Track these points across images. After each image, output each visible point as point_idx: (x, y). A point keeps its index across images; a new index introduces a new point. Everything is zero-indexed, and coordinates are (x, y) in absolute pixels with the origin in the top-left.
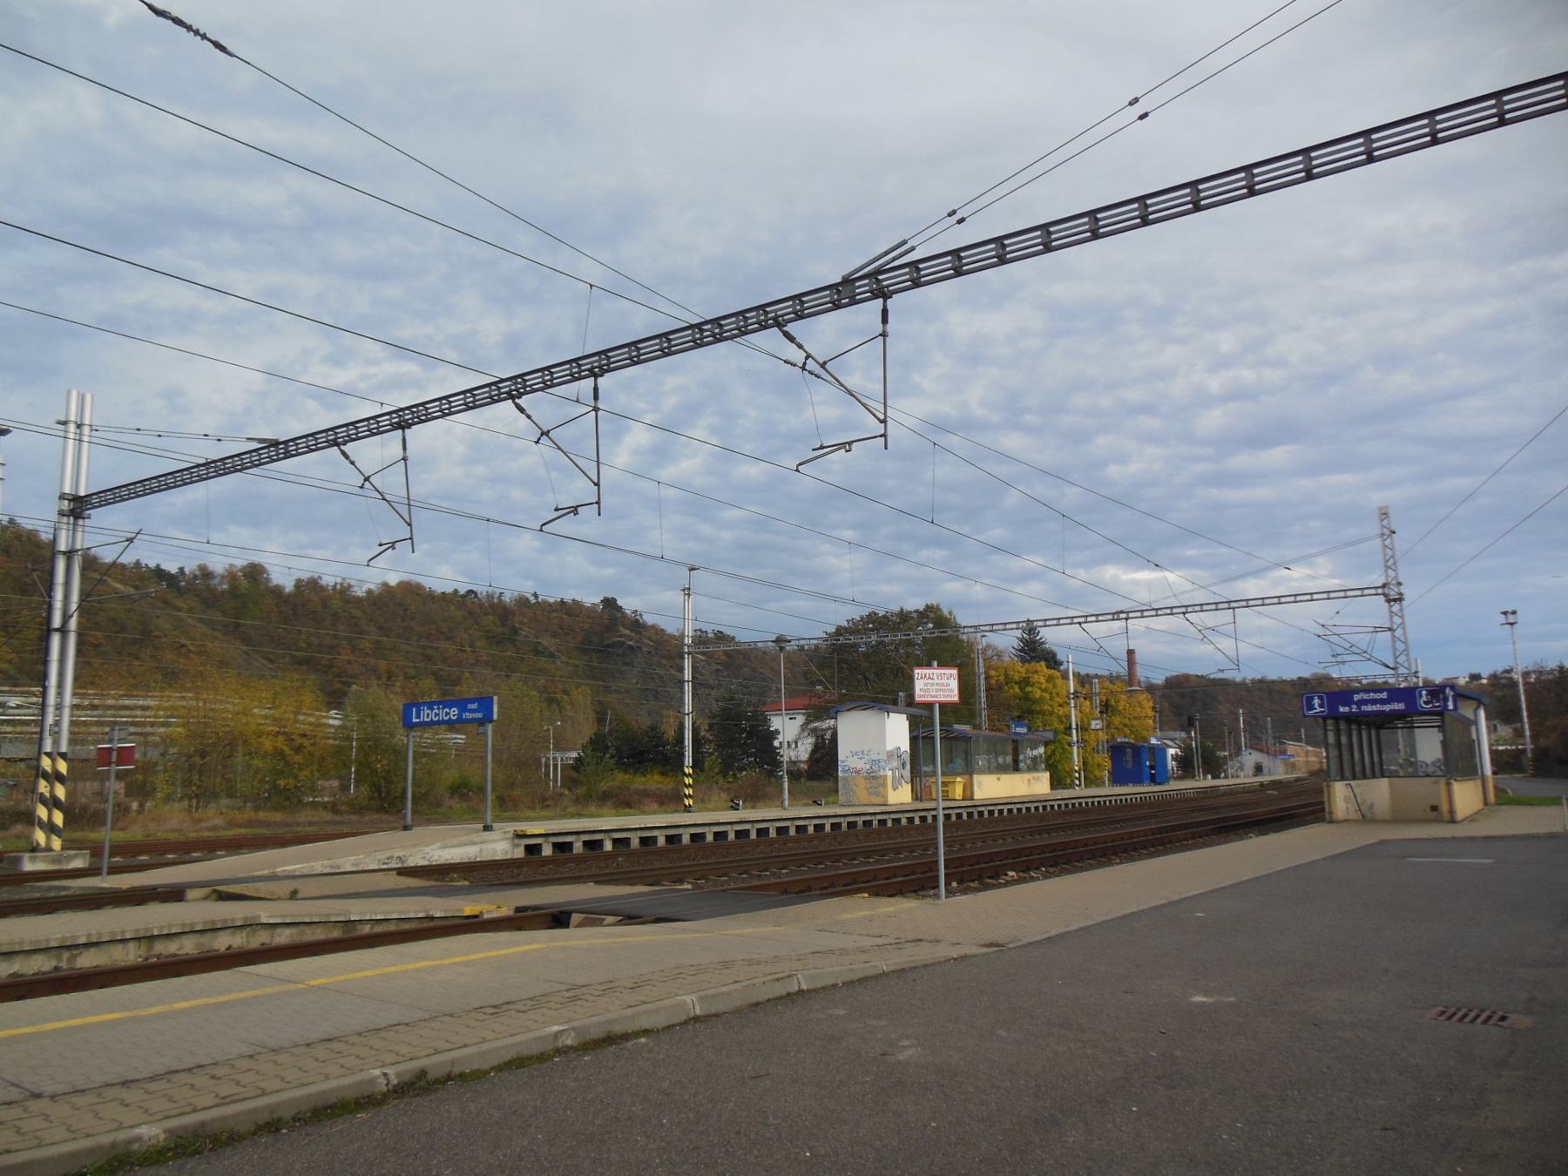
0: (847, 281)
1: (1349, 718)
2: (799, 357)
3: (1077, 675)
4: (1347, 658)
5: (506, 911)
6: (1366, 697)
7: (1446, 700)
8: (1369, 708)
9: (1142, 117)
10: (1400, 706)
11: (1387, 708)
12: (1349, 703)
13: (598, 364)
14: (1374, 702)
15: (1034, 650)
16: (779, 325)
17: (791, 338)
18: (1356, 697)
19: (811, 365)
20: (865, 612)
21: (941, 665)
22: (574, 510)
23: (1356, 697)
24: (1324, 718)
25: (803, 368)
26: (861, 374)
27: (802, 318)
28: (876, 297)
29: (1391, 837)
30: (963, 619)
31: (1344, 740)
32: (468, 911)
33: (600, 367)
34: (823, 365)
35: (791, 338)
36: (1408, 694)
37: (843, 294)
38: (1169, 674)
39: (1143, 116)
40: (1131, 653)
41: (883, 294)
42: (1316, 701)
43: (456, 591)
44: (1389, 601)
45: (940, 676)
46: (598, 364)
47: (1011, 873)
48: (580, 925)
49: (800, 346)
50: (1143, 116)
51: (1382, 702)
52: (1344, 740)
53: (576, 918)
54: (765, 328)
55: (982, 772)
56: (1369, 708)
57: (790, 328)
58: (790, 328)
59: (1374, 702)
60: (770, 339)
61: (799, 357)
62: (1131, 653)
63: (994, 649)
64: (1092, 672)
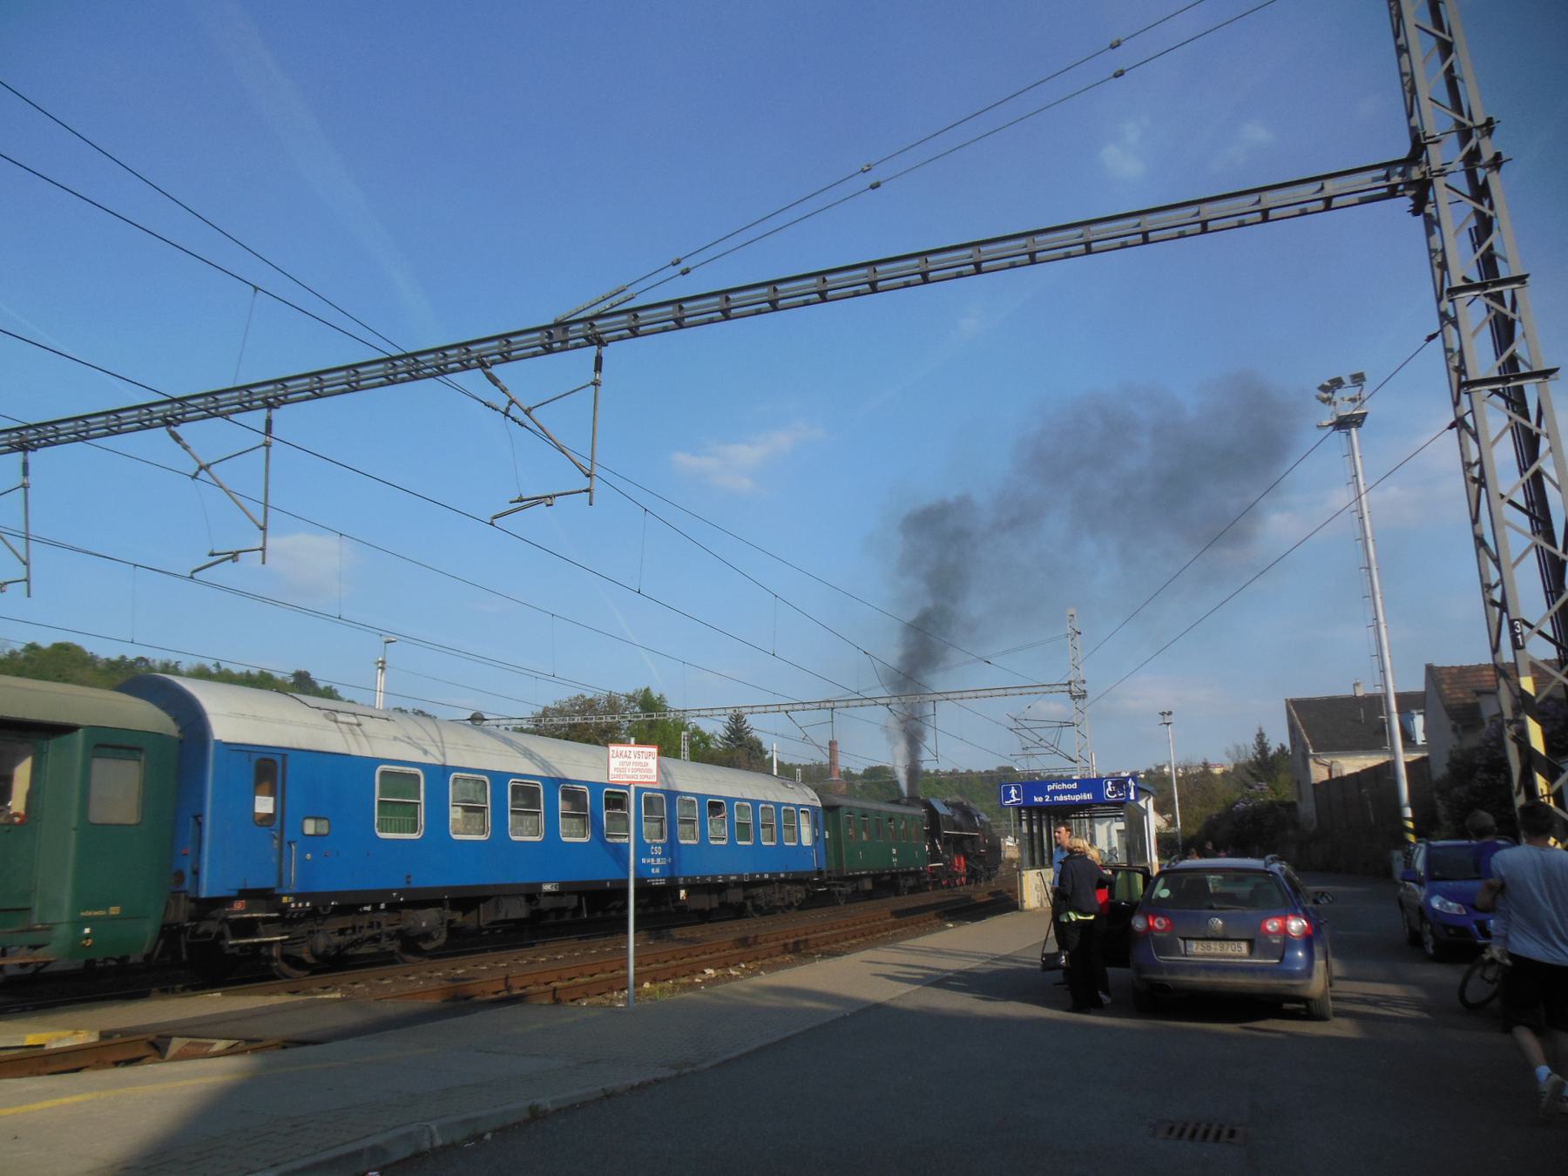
0: (563, 325)
1: (1042, 809)
2: (502, 401)
3: (780, 765)
4: (1034, 751)
5: (86, 1037)
6: (1058, 787)
7: (1128, 790)
8: (1061, 798)
9: (874, 187)
10: (1088, 796)
11: (1077, 798)
12: (1043, 793)
13: (273, 395)
14: (1065, 792)
15: (741, 739)
16: (482, 365)
17: (495, 381)
18: (1050, 788)
19: (515, 411)
20: (574, 693)
21: (639, 743)
22: (234, 556)
23: (1050, 788)
24: (1020, 808)
25: (506, 414)
26: (567, 421)
27: (507, 360)
28: (592, 344)
29: (1381, 986)
30: (674, 702)
31: (1035, 829)
32: (31, 1040)
33: (275, 397)
34: (527, 412)
35: (495, 381)
36: (1094, 785)
37: (552, 338)
38: (874, 764)
39: (875, 186)
40: (832, 744)
41: (597, 340)
42: (1013, 791)
43: (123, 658)
44: (1074, 698)
45: (638, 755)
46: (273, 395)
47: (709, 971)
48: (181, 1056)
49: (504, 390)
50: (875, 186)
51: (1072, 792)
52: (1035, 829)
53: (176, 1044)
54: (467, 368)
55: (1486, 667)
56: (1061, 798)
57: (496, 370)
58: (496, 370)
59: (1065, 792)
60: (473, 379)
61: (502, 401)
62: (832, 744)
63: (701, 734)
64: (796, 762)
